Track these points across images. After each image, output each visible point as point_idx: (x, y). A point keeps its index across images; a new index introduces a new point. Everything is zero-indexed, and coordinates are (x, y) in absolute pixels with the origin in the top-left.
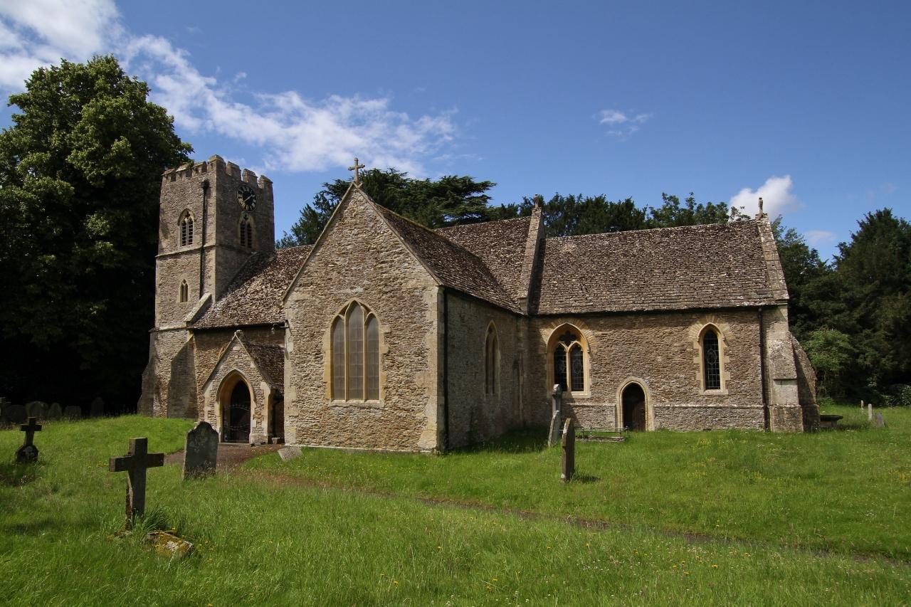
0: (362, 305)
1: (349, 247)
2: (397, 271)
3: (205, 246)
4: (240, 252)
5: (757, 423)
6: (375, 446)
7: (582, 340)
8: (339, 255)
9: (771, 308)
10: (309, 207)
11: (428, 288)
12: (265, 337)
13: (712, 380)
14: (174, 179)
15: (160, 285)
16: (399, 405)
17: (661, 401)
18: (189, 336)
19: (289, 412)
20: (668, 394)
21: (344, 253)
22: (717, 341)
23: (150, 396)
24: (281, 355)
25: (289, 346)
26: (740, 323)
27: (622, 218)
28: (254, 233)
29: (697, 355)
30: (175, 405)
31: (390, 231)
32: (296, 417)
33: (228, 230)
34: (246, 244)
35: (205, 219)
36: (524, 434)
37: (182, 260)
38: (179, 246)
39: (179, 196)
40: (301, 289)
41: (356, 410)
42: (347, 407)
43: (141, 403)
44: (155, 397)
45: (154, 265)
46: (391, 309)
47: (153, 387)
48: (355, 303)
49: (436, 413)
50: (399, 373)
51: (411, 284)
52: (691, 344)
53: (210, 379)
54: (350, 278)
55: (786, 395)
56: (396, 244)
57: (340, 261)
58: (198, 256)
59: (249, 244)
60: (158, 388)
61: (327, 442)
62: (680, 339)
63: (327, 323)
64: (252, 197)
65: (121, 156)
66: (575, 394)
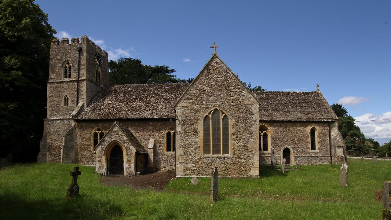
0: (220, 110)
1: (213, 83)
2: (238, 96)
3: (79, 79)
4: (96, 84)
5: (328, 162)
6: (227, 175)
7: (267, 131)
8: (207, 87)
9: (333, 122)
11: (254, 105)
15: (50, 97)
16: (240, 157)
18: (74, 124)
20: (299, 152)
21: (209, 86)
22: (315, 133)
23: (45, 153)
25: (179, 129)
26: (323, 127)
28: (101, 76)
30: (67, 157)
31: (235, 78)
32: (183, 163)
33: (91, 73)
34: (98, 81)
38: (62, 78)
40: (185, 101)
41: (217, 159)
42: (212, 158)
43: (40, 156)
44: (47, 153)
45: (47, 86)
47: (46, 148)
48: (216, 110)
49: (259, 160)
50: (240, 142)
51: (246, 102)
52: (307, 134)
54: (214, 98)
55: (340, 152)
56: (238, 84)
57: (208, 89)
58: (76, 84)
59: (99, 81)
60: (49, 149)
61: (200, 175)
63: (201, 118)
64: (100, 59)
65: (26, 28)
66: (265, 152)
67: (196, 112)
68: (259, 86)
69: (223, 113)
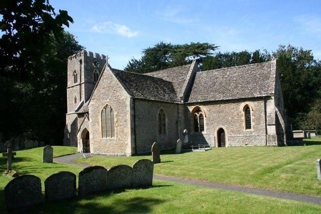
10: (130, 63)
13: (248, 126)
14: (71, 60)
20: (232, 131)
35: (81, 73)
39: (75, 65)
48: (107, 105)
51: (123, 98)
52: (241, 112)
68: (60, 11)
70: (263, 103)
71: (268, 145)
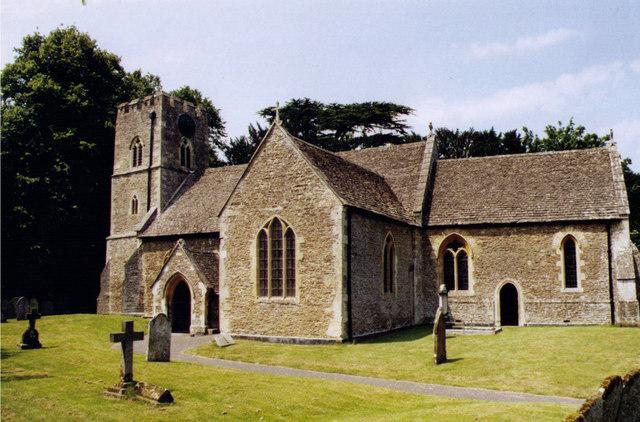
12: (202, 243)
13: (571, 281)
14: (127, 111)
16: (312, 302)
17: (531, 298)
19: (224, 307)
22: (574, 249)
24: (215, 261)
25: (222, 254)
27: (512, 144)
28: (192, 154)
29: (559, 260)
36: (404, 328)
37: (132, 179)
46: (305, 224)
51: (321, 204)
52: (554, 251)
53: (157, 279)
58: (146, 175)
62: (546, 246)
67: (247, 224)
69: (287, 225)
70: (605, 234)
71: (618, 320)
